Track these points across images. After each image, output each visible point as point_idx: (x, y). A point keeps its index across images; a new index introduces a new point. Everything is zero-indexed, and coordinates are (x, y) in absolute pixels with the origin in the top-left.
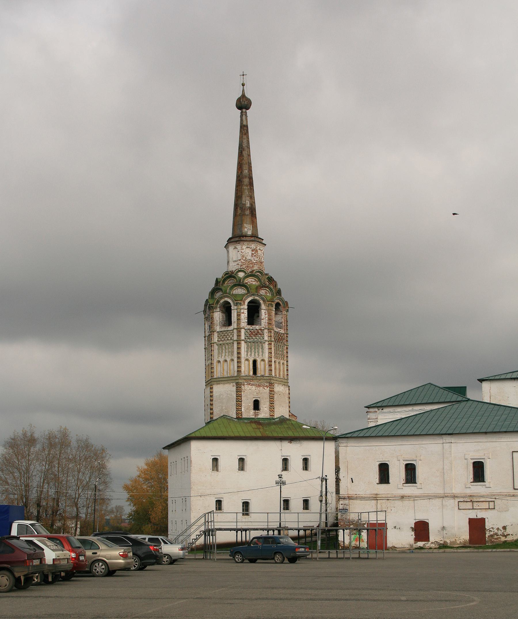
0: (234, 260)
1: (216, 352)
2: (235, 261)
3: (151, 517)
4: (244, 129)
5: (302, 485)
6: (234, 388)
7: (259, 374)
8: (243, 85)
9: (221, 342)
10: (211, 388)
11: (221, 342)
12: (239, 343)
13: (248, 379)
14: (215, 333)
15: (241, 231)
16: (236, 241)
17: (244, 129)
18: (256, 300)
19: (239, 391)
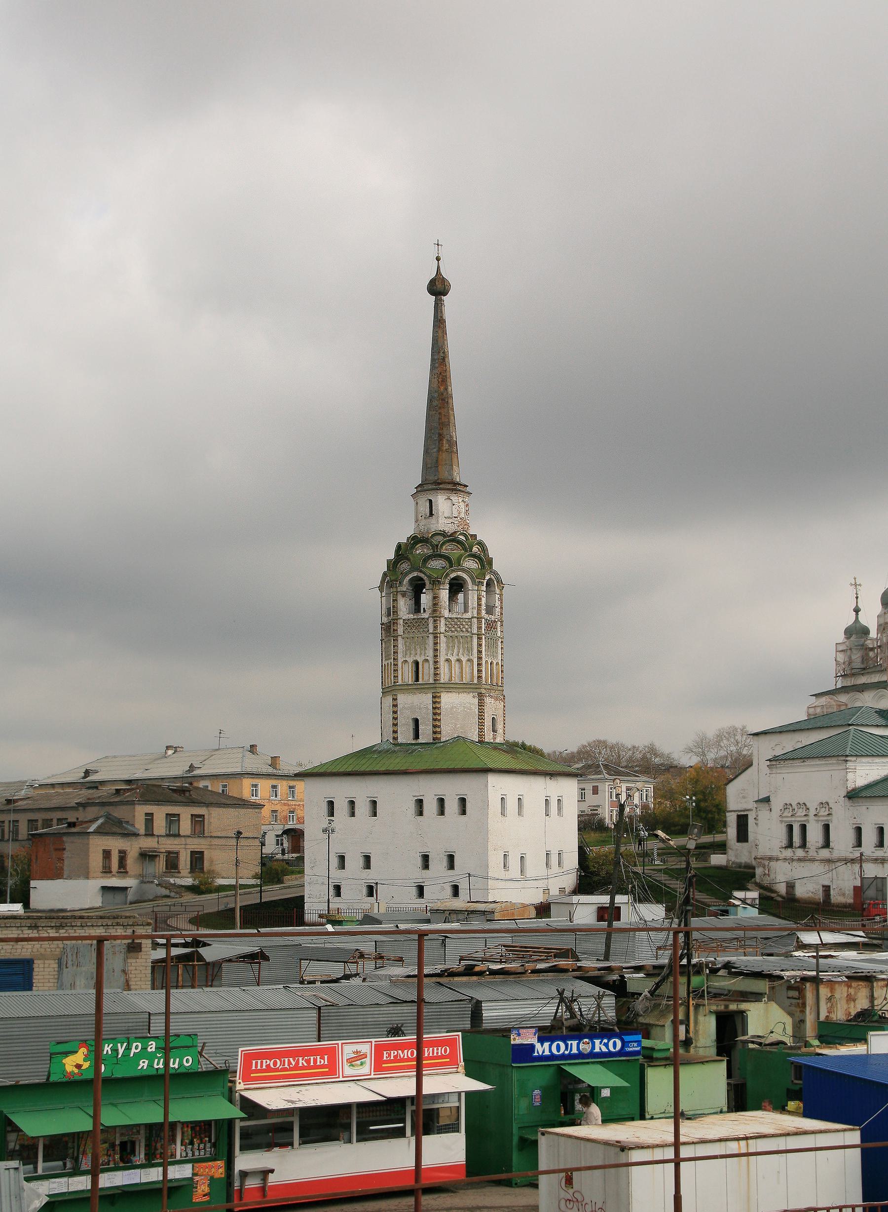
0: (446, 515)
1: (443, 646)
2: (449, 518)
3: (397, 897)
4: (439, 322)
5: (110, 931)
6: (476, 700)
7: (421, 681)
8: (438, 259)
9: (450, 634)
10: (395, 700)
11: (450, 634)
12: (479, 639)
13: (406, 688)
14: (442, 619)
15: (451, 475)
16: (448, 489)
17: (439, 322)
18: (458, 576)
19: (481, 704)
